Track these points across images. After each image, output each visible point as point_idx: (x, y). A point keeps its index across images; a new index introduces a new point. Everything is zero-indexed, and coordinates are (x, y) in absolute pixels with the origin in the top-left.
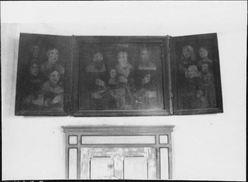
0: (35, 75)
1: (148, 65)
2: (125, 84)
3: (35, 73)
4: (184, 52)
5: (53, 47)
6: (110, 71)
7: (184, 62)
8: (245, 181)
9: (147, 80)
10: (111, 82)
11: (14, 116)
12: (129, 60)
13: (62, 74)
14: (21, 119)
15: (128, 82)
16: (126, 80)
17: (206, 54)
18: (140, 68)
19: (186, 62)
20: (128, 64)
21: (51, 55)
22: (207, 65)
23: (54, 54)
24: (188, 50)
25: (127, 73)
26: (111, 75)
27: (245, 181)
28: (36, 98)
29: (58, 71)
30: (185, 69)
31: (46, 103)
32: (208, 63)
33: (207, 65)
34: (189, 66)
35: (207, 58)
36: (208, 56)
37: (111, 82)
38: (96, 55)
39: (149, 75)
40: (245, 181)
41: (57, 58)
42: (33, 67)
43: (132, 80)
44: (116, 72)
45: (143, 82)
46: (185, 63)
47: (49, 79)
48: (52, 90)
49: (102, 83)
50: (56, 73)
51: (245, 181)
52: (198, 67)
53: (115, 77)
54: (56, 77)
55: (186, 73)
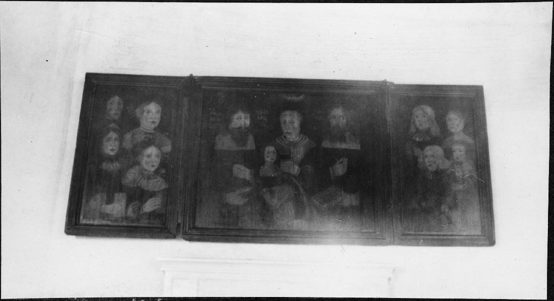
0: (112, 153)
1: (342, 139)
2: (294, 176)
3: (112, 150)
4: (417, 117)
5: (149, 99)
6: (264, 150)
7: (416, 137)
8: (2, 298)
9: (340, 169)
10: (267, 170)
11: (65, 235)
12: (304, 129)
13: (167, 154)
14: (72, 238)
15: (302, 174)
16: (296, 170)
17: (461, 126)
18: (326, 144)
19: (420, 138)
20: (302, 135)
21: (145, 114)
22: (462, 148)
23: (151, 114)
24: (425, 114)
25: (299, 153)
26: (266, 157)
27: (545, 298)
28: (110, 201)
29: (159, 147)
30: (417, 151)
31: (130, 209)
32: (463, 143)
33: (462, 148)
34: (427, 145)
35: (462, 134)
36: (465, 130)
37: (267, 170)
38: (236, 116)
39: (345, 161)
40: (2, 298)
41: (157, 121)
42: (109, 140)
43: (309, 168)
44: (275, 151)
45: (331, 172)
46: (417, 139)
47: (138, 163)
48: (144, 184)
49: (243, 172)
50: (152, 151)
51: (545, 298)
52: (445, 151)
53: (273, 161)
54: (153, 158)
55: (420, 160)
